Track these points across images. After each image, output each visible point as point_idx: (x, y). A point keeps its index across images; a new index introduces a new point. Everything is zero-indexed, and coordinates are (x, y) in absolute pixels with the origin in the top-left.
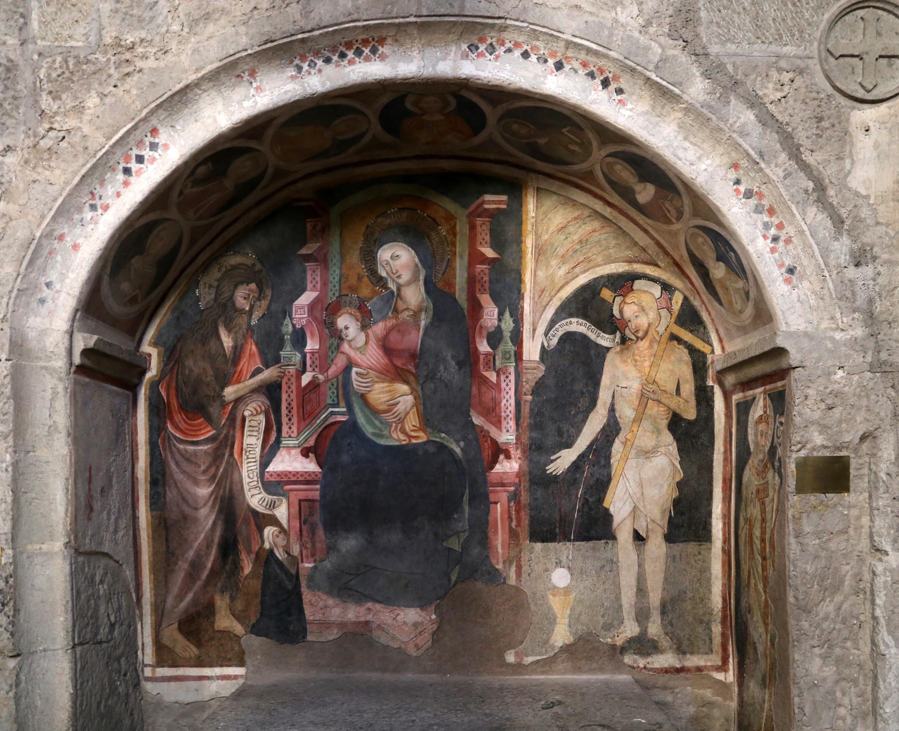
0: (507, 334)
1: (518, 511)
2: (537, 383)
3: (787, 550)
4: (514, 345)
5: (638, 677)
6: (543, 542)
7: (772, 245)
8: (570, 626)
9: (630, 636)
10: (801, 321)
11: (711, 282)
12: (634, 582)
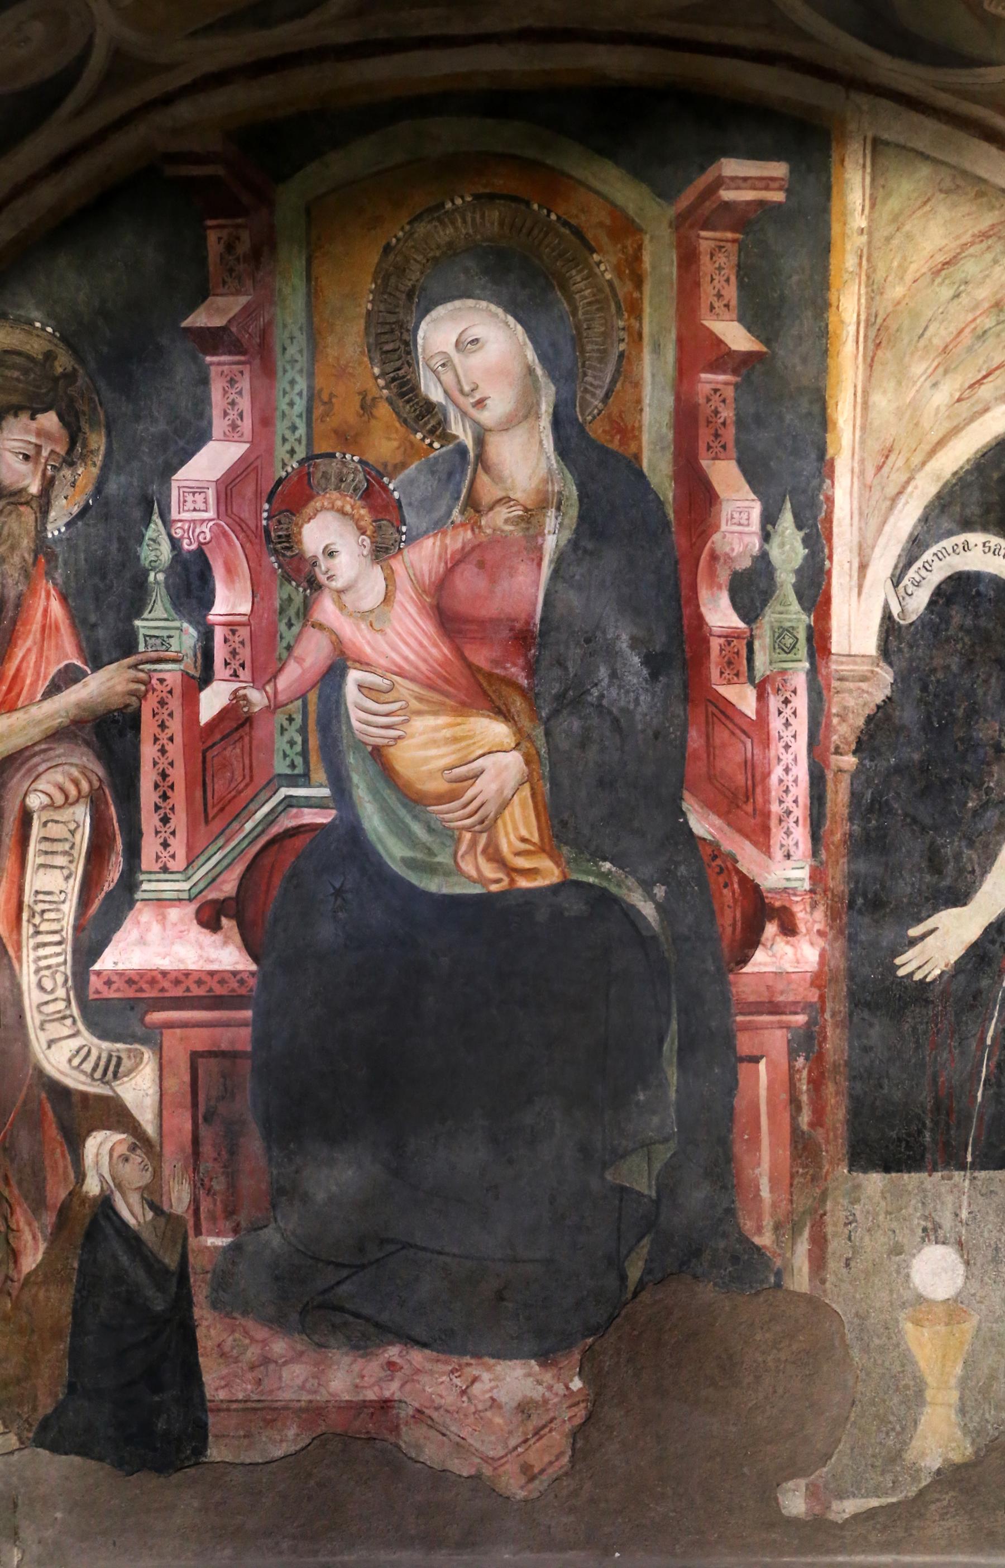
0: (786, 578)
1: (816, 1084)
2: (869, 719)
4: (807, 610)
6: (887, 1170)
8: (962, 1411)
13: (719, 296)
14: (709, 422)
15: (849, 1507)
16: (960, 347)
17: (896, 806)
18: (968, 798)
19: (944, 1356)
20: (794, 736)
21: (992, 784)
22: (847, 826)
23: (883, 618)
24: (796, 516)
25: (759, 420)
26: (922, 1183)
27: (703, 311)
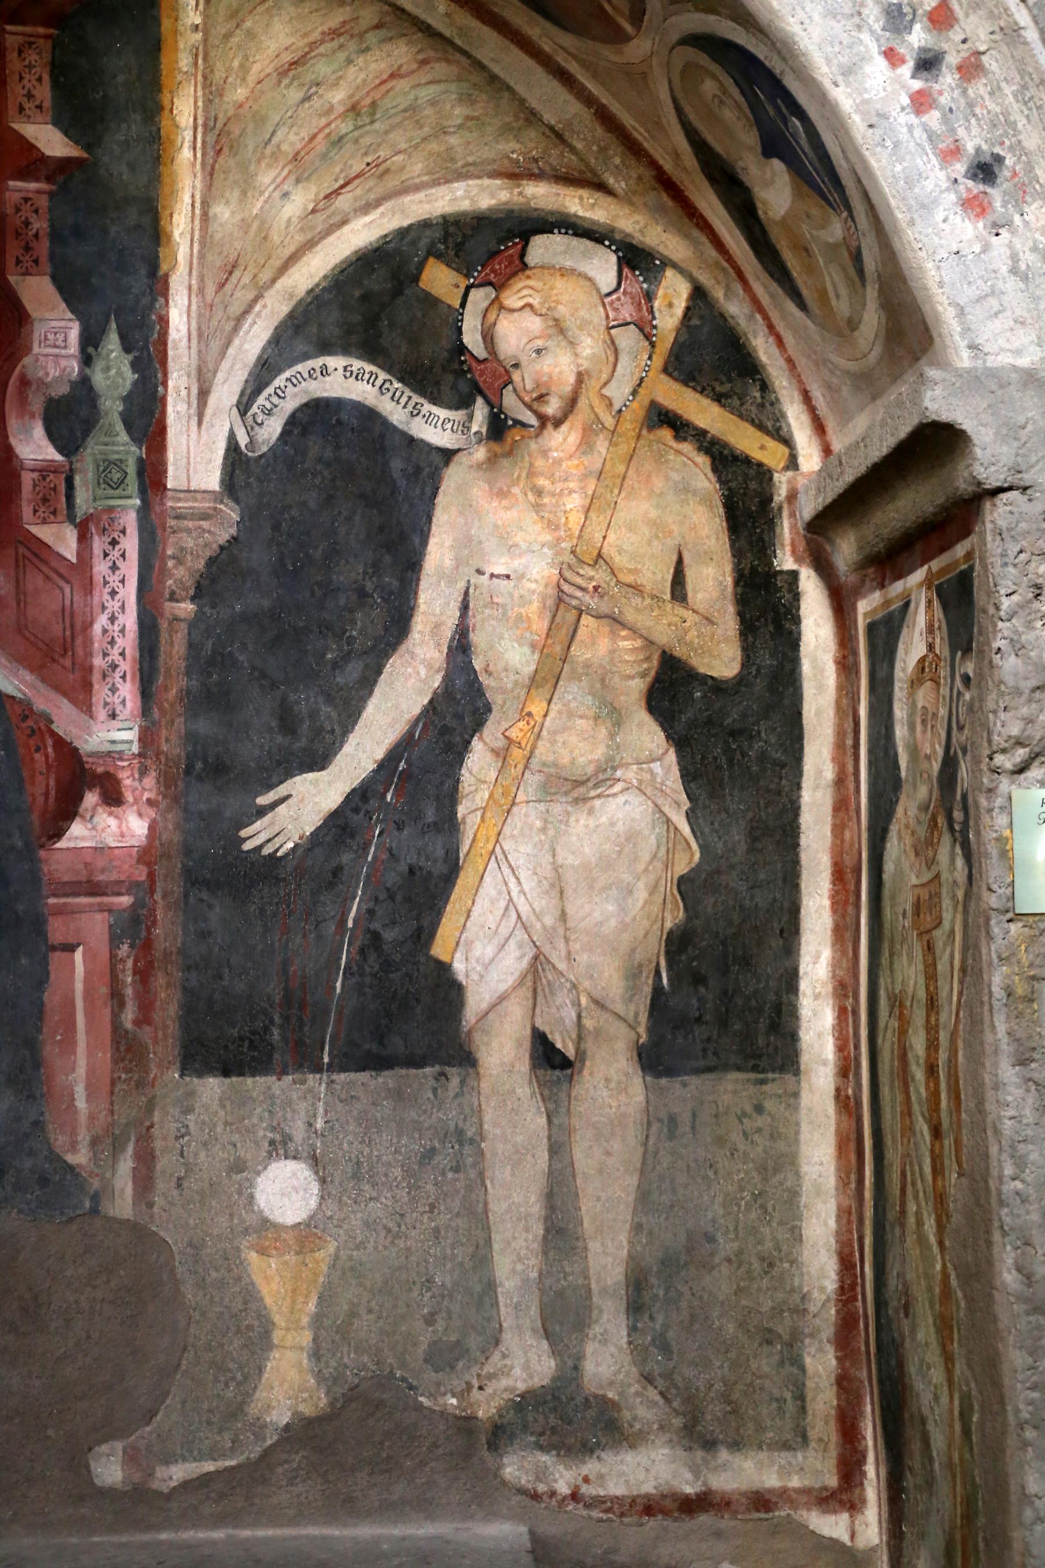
0: (112, 407)
1: (144, 975)
2: (211, 561)
3: (990, 1106)
4: (137, 440)
5: (549, 1529)
6: (226, 1073)
7: (917, 85)
8: (316, 1354)
9: (521, 1387)
10: (1025, 338)
11: (764, 232)
12: (536, 1208)
13: (30, 96)
14: (18, 234)
15: (178, 1473)
16: (312, 154)
17: (241, 658)
18: (327, 649)
19: (294, 1291)
20: (123, 581)
21: (354, 633)
22: (184, 682)
23: (228, 450)
24: (123, 337)
25: (78, 232)
26: (269, 1088)
27: (11, 113)
